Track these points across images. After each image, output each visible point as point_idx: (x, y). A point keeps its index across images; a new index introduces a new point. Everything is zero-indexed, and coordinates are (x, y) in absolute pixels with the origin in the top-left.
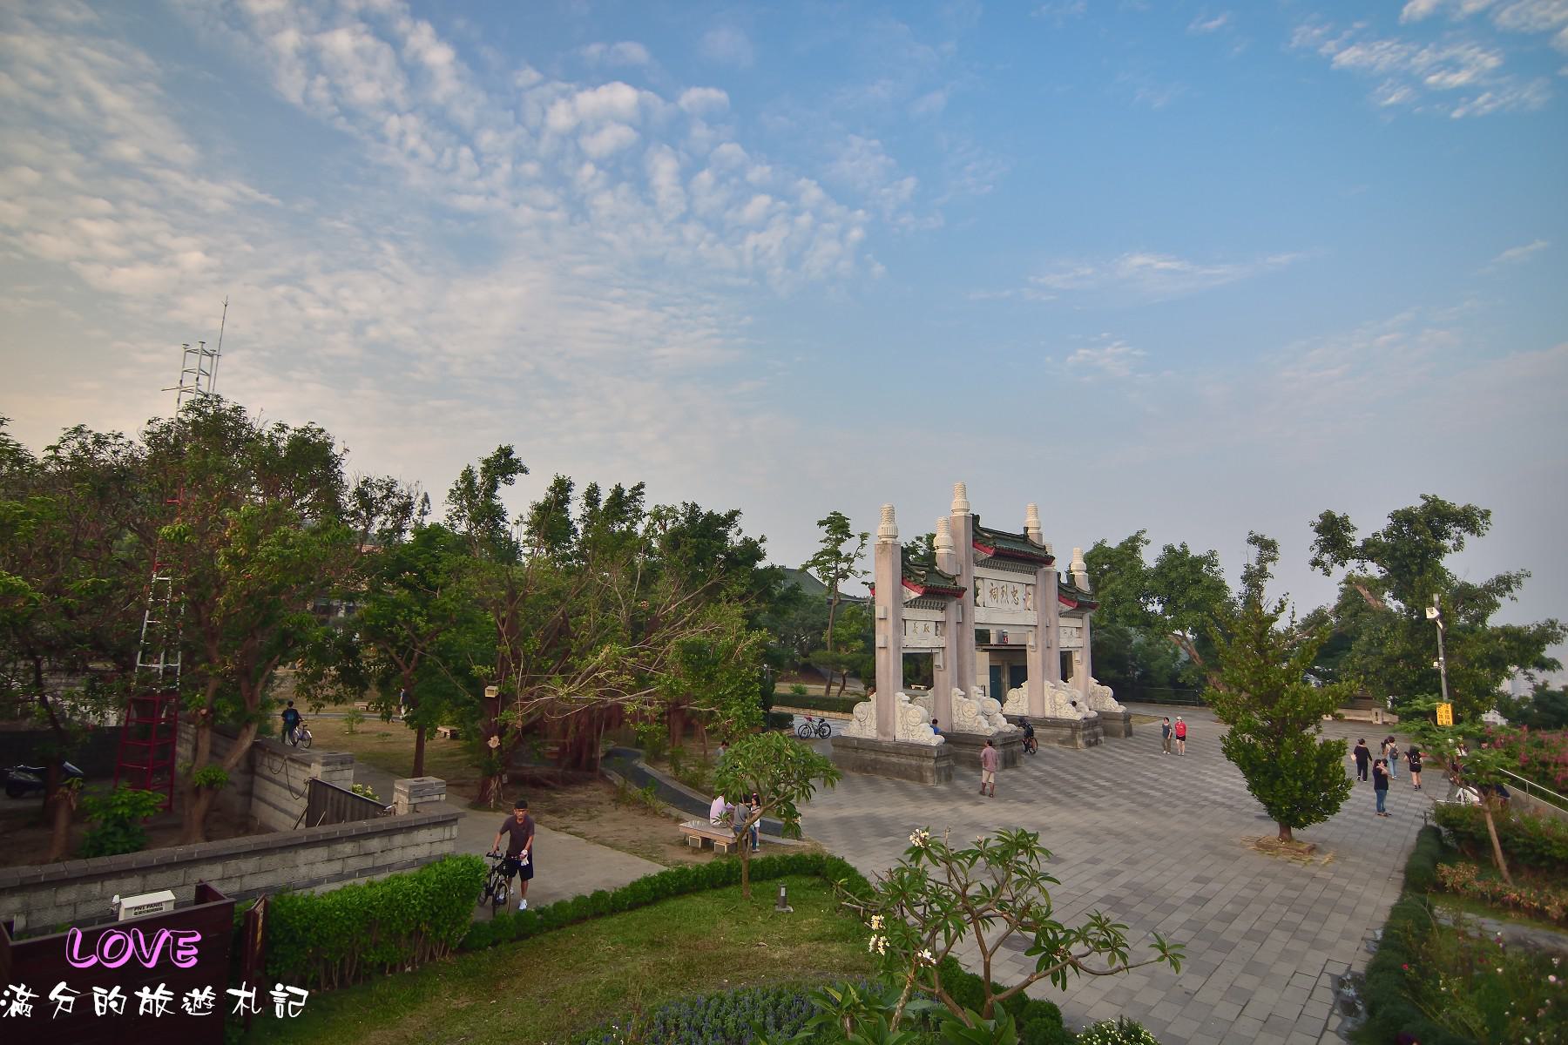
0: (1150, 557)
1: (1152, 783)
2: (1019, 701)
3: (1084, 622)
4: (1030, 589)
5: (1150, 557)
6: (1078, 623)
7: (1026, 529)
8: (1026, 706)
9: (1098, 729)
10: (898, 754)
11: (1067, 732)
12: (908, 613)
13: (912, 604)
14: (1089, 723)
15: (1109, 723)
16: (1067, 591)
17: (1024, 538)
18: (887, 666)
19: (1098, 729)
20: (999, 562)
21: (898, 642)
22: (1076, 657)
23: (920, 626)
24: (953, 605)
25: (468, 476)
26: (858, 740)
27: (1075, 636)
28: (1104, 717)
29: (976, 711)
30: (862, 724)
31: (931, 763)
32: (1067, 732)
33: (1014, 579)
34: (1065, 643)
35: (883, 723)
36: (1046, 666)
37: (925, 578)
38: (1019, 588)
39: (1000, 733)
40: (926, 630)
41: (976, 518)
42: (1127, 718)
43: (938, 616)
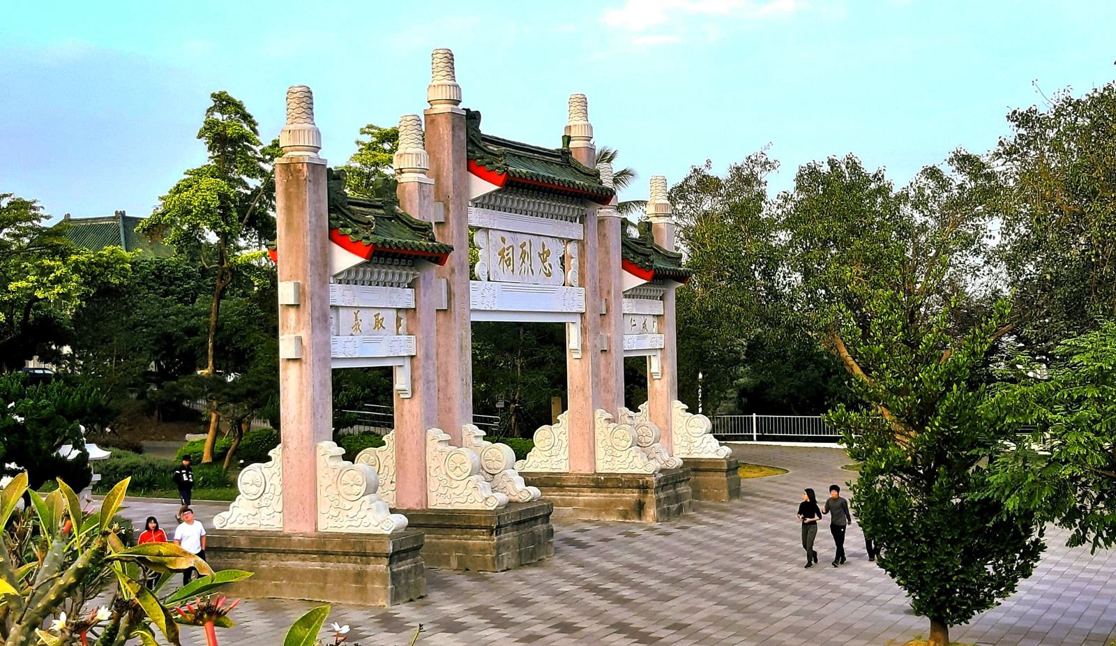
0: (779, 186)
1: (755, 571)
2: (553, 448)
3: (666, 307)
4: (572, 249)
5: (779, 186)
6: (657, 307)
7: (567, 139)
8: (564, 455)
9: (683, 489)
10: (324, 554)
11: (632, 496)
12: (339, 294)
13: (348, 278)
14: (670, 479)
15: (702, 477)
16: (640, 253)
17: (564, 157)
18: (300, 396)
19: (680, 489)
20: (515, 200)
21: (323, 351)
22: (654, 366)
23: (367, 318)
24: (435, 279)
25: (226, 92)
26: (338, 535)
27: (650, 331)
28: (694, 467)
29: (466, 471)
30: (258, 501)
31: (382, 566)
32: (632, 496)
33: (549, 229)
34: (634, 343)
35: (823, 503)
36: (598, 382)
37: (381, 230)
38: (552, 246)
39: (510, 504)
40: (379, 324)
41: (473, 118)
42: (732, 467)
43: (405, 297)
